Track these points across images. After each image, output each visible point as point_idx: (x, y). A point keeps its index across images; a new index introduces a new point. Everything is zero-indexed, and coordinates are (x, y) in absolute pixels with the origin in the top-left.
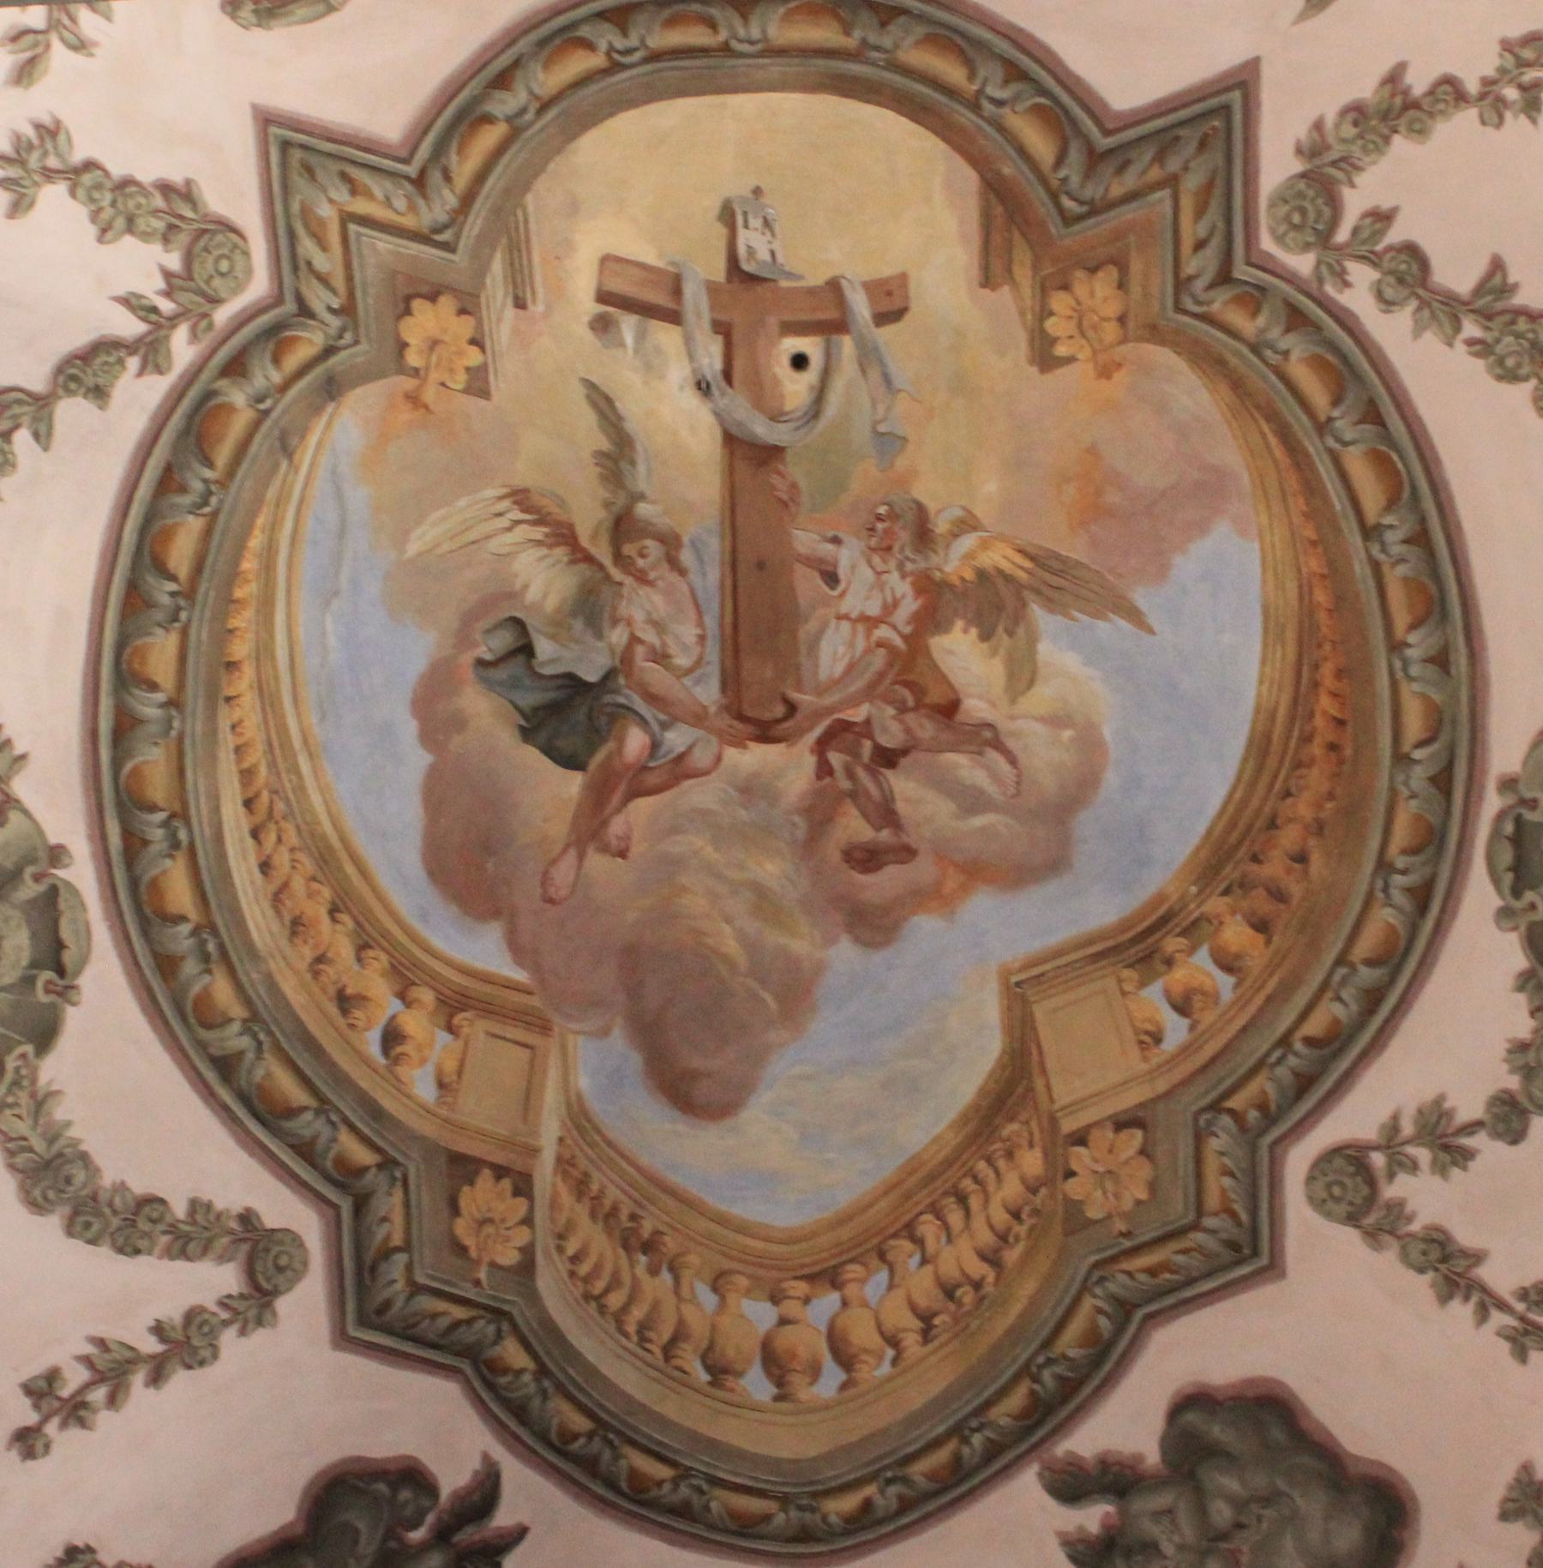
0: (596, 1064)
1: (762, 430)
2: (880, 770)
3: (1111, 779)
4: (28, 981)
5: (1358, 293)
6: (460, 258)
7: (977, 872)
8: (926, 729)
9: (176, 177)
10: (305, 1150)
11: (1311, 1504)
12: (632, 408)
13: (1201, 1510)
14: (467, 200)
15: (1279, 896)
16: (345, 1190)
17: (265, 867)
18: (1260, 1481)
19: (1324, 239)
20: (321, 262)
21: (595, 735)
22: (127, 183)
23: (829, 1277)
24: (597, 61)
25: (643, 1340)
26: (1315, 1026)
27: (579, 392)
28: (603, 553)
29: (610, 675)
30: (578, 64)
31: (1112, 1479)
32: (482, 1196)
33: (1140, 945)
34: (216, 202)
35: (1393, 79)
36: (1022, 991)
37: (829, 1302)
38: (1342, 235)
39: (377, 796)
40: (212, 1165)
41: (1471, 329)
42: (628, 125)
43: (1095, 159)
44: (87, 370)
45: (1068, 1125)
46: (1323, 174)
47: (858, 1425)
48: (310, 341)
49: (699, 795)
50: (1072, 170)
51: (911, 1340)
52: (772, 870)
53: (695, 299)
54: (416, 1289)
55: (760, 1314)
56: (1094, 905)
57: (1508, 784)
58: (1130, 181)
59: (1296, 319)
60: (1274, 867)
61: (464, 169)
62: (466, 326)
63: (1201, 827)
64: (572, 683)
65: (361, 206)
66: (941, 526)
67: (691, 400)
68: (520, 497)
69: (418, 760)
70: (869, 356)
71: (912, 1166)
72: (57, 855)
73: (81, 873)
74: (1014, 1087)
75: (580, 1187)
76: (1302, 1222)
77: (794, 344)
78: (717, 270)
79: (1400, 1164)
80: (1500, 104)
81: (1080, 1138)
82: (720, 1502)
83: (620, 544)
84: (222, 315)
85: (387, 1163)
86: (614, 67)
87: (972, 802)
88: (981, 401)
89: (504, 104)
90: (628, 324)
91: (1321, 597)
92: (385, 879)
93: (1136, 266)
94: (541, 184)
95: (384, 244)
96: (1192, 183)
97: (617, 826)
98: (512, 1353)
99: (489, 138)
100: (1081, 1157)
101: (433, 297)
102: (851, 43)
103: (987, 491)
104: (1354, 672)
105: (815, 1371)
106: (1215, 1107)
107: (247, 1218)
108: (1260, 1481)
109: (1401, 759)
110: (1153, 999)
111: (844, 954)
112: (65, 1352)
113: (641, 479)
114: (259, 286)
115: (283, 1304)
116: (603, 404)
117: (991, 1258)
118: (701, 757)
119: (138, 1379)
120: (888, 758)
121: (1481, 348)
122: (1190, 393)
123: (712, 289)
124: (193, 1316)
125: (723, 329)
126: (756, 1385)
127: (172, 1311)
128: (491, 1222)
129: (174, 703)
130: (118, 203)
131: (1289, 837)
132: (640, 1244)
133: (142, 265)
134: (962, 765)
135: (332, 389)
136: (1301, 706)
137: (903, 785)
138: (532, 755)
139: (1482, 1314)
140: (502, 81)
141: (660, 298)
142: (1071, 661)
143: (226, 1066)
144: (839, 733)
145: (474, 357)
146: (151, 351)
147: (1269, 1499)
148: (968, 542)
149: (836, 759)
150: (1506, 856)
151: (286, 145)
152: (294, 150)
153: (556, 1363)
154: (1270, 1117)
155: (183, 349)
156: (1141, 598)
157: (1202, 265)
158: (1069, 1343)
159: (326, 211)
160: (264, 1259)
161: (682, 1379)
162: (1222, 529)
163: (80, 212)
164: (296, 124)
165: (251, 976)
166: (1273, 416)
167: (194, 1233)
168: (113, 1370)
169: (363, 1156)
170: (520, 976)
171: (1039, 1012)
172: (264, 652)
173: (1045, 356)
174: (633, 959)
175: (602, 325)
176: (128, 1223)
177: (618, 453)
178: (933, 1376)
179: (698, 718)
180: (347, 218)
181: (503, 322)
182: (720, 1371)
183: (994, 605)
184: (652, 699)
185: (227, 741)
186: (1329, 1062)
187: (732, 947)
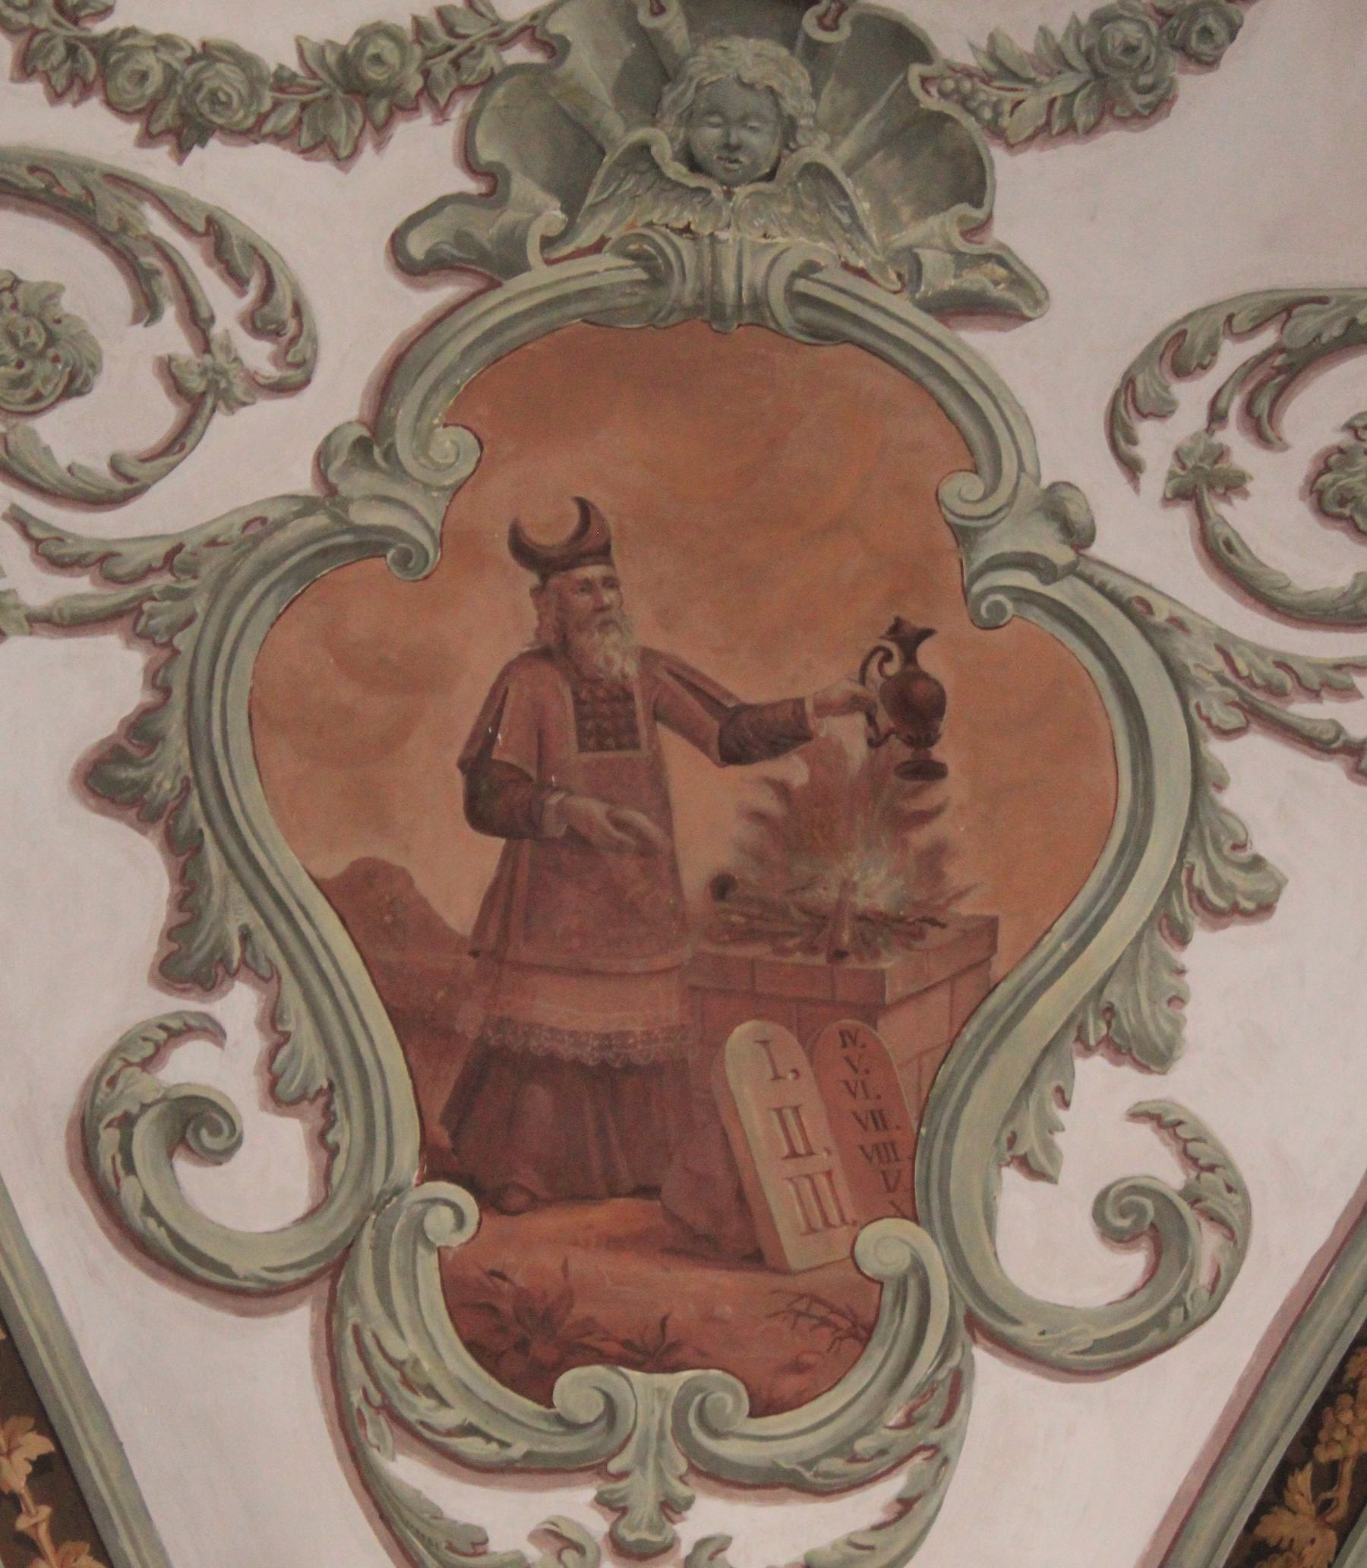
4: (814, 52)
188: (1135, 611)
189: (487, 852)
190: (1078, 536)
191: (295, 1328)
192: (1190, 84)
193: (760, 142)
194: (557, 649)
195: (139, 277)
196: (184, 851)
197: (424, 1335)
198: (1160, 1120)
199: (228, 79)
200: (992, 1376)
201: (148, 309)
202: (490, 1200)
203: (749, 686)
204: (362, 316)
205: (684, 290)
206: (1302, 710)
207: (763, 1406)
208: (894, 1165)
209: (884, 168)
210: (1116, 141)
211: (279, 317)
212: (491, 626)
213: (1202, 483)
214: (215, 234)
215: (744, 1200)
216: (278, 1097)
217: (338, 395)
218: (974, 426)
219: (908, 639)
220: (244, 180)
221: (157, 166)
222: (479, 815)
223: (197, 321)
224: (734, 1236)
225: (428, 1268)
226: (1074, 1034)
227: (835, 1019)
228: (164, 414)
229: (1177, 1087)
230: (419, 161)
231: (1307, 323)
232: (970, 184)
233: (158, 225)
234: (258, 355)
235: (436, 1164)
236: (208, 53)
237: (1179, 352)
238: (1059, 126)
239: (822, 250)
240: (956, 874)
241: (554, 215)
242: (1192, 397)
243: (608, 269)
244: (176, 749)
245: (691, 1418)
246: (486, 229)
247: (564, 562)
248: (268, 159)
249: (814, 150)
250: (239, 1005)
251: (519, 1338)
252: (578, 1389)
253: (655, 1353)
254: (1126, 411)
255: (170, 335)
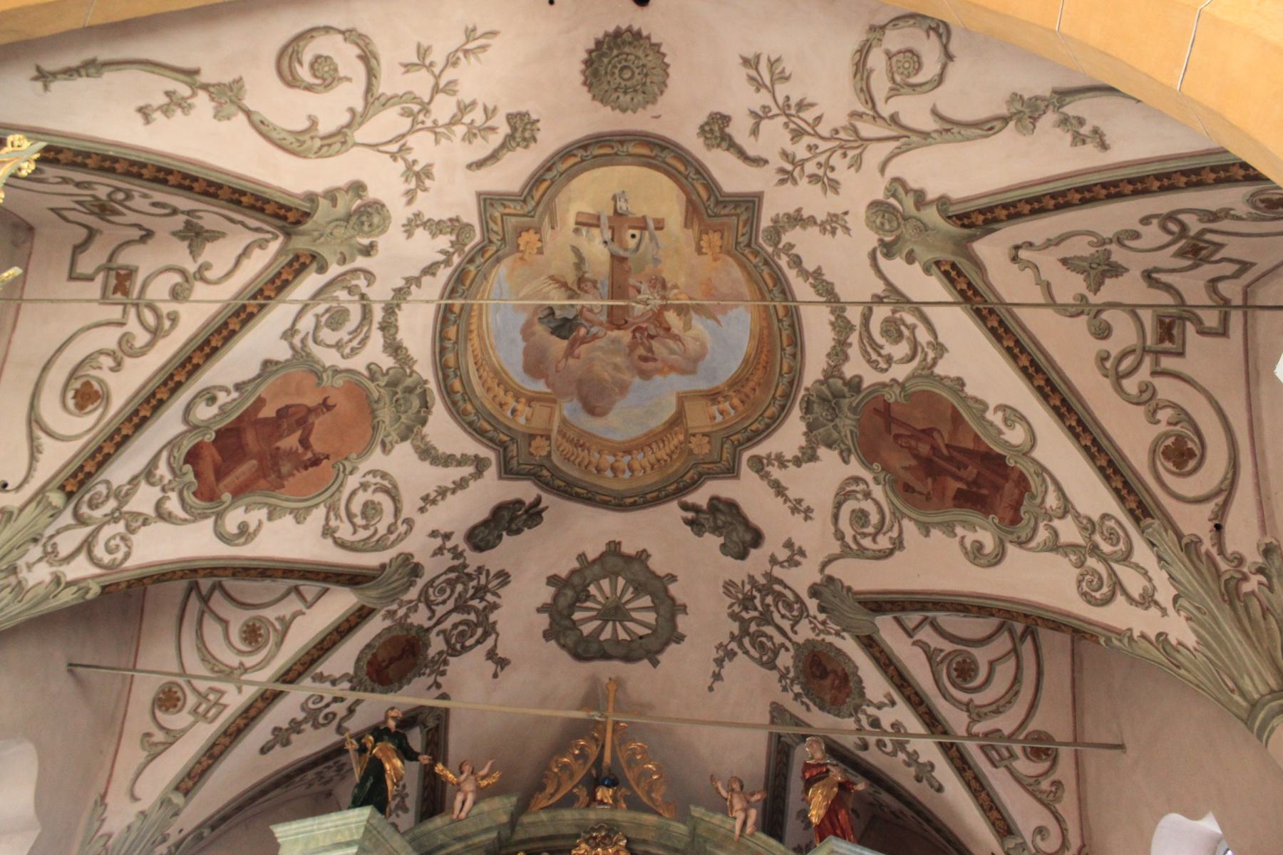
0: (569, 409)
1: (622, 253)
2: (648, 342)
3: (708, 357)
4: (419, 412)
5: (783, 262)
6: (536, 219)
7: (673, 368)
8: (662, 332)
9: (453, 216)
10: (491, 440)
11: (741, 529)
12: (585, 251)
13: (715, 522)
14: (538, 204)
15: (747, 396)
16: (501, 447)
17: (480, 377)
18: (729, 519)
19: (776, 245)
20: (495, 228)
21: (571, 331)
22: (440, 222)
23: (628, 452)
24: (578, 159)
25: (579, 465)
26: (754, 427)
27: (569, 249)
28: (575, 288)
29: (576, 317)
30: (572, 161)
31: (695, 508)
32: (537, 442)
33: (713, 396)
34: (465, 220)
35: (799, 210)
36: (682, 399)
37: (628, 458)
38: (781, 246)
39: (510, 357)
40: (468, 445)
41: (811, 280)
42: (585, 176)
43: (718, 203)
44: (430, 270)
45: (691, 431)
46: (776, 231)
47: (634, 484)
48: (493, 249)
49: (598, 343)
50: (712, 203)
51: (648, 469)
52: (618, 360)
53: (604, 221)
54: (519, 464)
55: (611, 459)
56: (703, 385)
57: (807, 389)
58: (726, 211)
59: (766, 263)
60: (747, 390)
61: (537, 195)
62: (537, 237)
63: (730, 375)
64: (566, 320)
65: (507, 211)
66: (669, 285)
67: (602, 246)
68: (552, 278)
69: (521, 344)
70: (652, 238)
71: (651, 431)
72: (426, 382)
73: (432, 385)
74: (677, 420)
75: (564, 436)
76: (745, 468)
77: (632, 231)
78: (611, 213)
79: (769, 463)
80: (825, 229)
81: (694, 435)
82: (598, 498)
83: (582, 284)
84: (467, 249)
85: (512, 439)
86: (583, 161)
87: (672, 352)
88: (681, 257)
89: (549, 175)
90: (584, 230)
91: (765, 332)
92: (512, 374)
93: (726, 234)
94: (560, 195)
95: (514, 220)
96: (743, 217)
97: (577, 352)
98: (545, 473)
99: (545, 185)
100: (693, 439)
101: (527, 231)
102: (653, 154)
103: (682, 280)
104: (771, 352)
105: (624, 472)
106: (727, 438)
107: (476, 456)
108: (729, 519)
109: (781, 375)
110: (714, 409)
111: (637, 380)
112: (431, 491)
113: (586, 267)
114: (478, 238)
115: (485, 473)
116: (576, 251)
117: (670, 456)
118: (601, 334)
119: (449, 494)
120: (651, 337)
121: (814, 286)
122: (737, 273)
123: (609, 218)
124: (462, 479)
125: (612, 228)
126: (609, 473)
127: (457, 478)
128: (540, 448)
129: (456, 342)
130: (436, 228)
131: (751, 384)
132: (578, 445)
133: (444, 241)
134: (671, 343)
135: (498, 260)
136: (758, 352)
137: (655, 344)
138: (554, 338)
139: (785, 502)
140: (549, 169)
141: (595, 222)
142: (701, 327)
143: (470, 424)
144: (638, 329)
145: (539, 244)
146: (447, 262)
147: (731, 524)
148: (676, 291)
149: (638, 335)
150: (804, 405)
151: (485, 200)
152: (487, 201)
153: (555, 472)
154: (740, 444)
155: (456, 260)
156: (719, 317)
157: (743, 240)
158: (687, 478)
159: (497, 214)
160: (480, 465)
161: (590, 473)
162: (741, 309)
163: (427, 233)
164: (489, 194)
165: (477, 403)
166: (757, 284)
167: (462, 461)
168: (442, 492)
169: (506, 438)
170: (549, 391)
171: (686, 404)
172: (480, 327)
173: (699, 250)
174: (580, 382)
175: (576, 231)
176: (447, 461)
177: (580, 261)
178: (652, 478)
179: (601, 324)
180: (503, 215)
181: (547, 233)
182: (599, 470)
183: (682, 310)
184: (587, 320)
185: (470, 349)
186: (755, 437)
187: (607, 377)
188: (341, 485)
189: (273, 414)
190: (351, 473)
191: (183, 428)
192: (427, 463)
193: (403, 408)
194: (310, 411)
195: (355, 330)
196: (259, 376)
197: (187, 445)
198: (260, 523)
199: (393, 331)
200: (210, 522)
201: (350, 333)
202: (214, 441)
203: (312, 439)
204: (358, 363)
205: (375, 406)
206: (332, 514)
207: (195, 494)
208: (238, 493)
209: (403, 427)
210: (416, 456)
211: (354, 351)
212: (311, 400)
213: (364, 486)
214: (366, 337)
215: (227, 474)
216: (221, 408)
217: (343, 364)
218: (365, 452)
219: (327, 457)
220: (377, 339)
221: (375, 325)
222: (278, 411)
223: (350, 341)
224: (220, 474)
225: (199, 439)
226: (269, 505)
227: (262, 473)
228: (333, 342)
229: (266, 524)
230: (387, 362)
231: (393, 491)
232: (403, 438)
233: (365, 329)
234: (347, 350)
235: (217, 432)
236: (396, 327)
237: (384, 475)
238: (416, 448)
239: (387, 422)
240: (291, 479)
241: (383, 384)
242: (378, 480)
243: (376, 395)
244: (274, 368)
245: (189, 485)
246: (378, 375)
247: (326, 406)
248: (382, 341)
249: (403, 417)
250: (235, 395)
251: (193, 456)
252: (188, 468)
253: (197, 475)
254: (373, 472)
255: (346, 338)
